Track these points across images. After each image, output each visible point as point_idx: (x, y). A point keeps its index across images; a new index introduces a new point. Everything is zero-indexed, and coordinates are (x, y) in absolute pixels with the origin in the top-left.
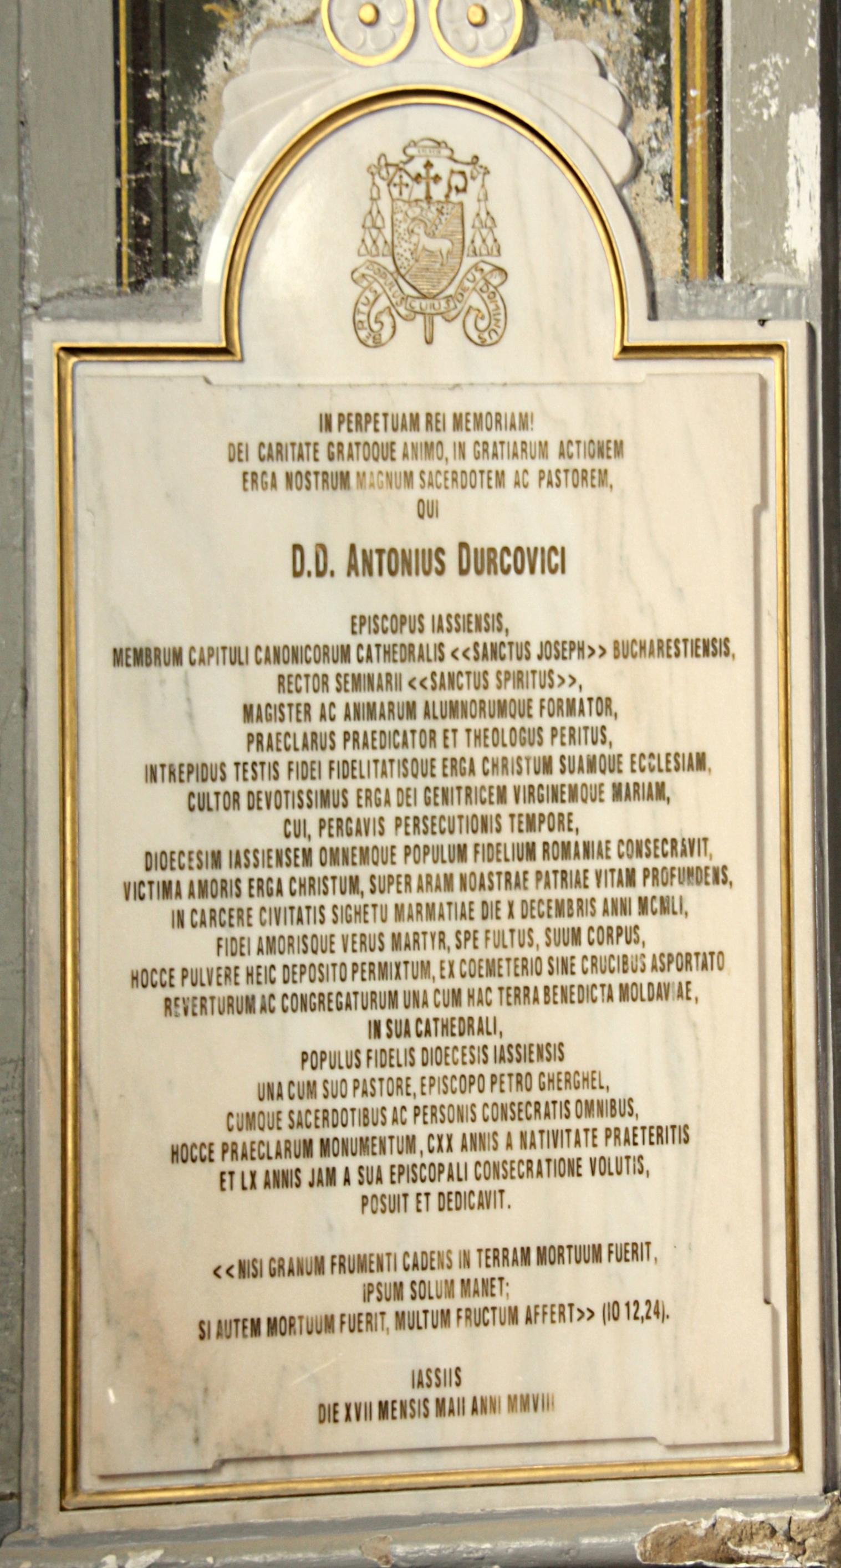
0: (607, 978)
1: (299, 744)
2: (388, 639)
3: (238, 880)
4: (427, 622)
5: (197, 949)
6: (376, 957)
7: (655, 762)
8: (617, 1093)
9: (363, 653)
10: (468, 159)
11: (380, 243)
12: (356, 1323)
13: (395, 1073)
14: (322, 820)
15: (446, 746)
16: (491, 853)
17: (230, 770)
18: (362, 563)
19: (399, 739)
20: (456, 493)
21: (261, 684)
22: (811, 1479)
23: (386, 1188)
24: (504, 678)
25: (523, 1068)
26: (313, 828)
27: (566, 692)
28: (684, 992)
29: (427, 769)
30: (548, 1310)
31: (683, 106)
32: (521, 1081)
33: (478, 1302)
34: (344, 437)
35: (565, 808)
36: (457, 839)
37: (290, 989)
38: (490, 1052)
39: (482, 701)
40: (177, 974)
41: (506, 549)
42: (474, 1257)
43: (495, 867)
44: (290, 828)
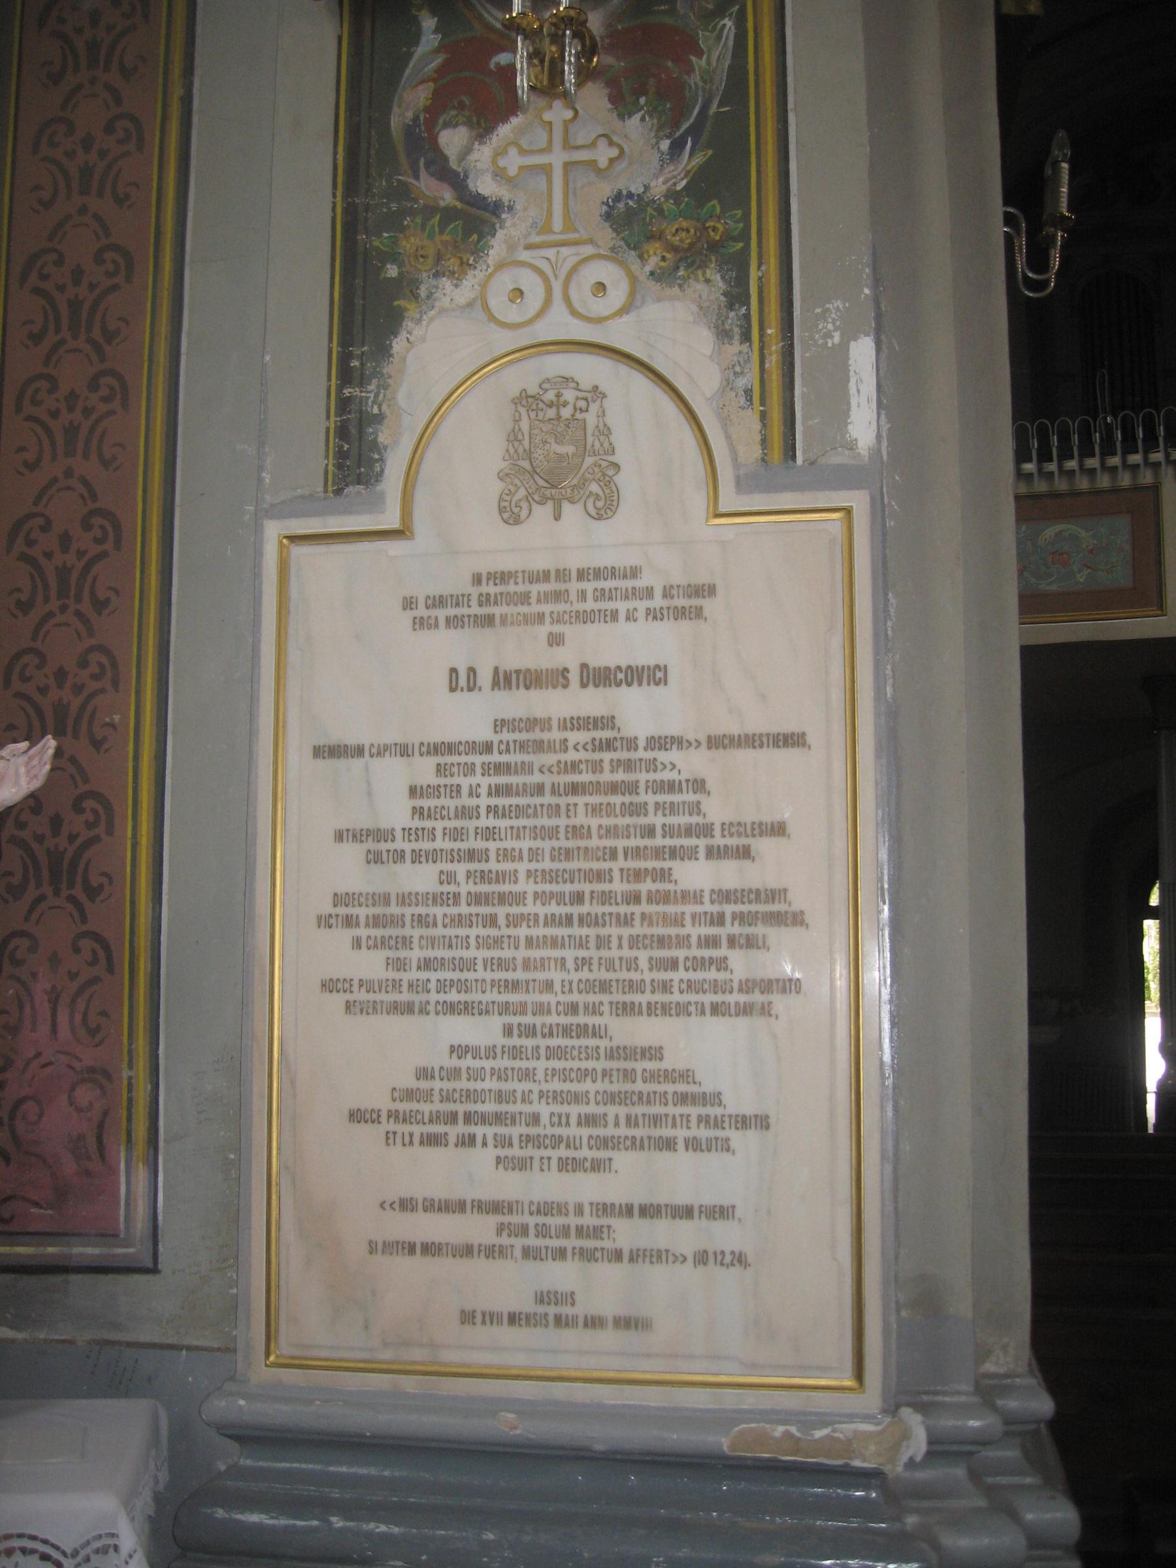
0: (701, 998)
1: (452, 814)
2: (524, 736)
3: (403, 915)
4: (555, 724)
5: (372, 965)
6: (510, 976)
7: (742, 829)
8: (708, 1087)
9: (503, 747)
10: (589, 388)
11: (521, 450)
12: (492, 1252)
13: (524, 1064)
14: (468, 872)
15: (568, 817)
16: (606, 898)
17: (399, 834)
18: (503, 680)
19: (530, 811)
20: (579, 628)
21: (425, 770)
22: (872, 1399)
23: (516, 1152)
24: (616, 765)
25: (629, 1065)
26: (461, 877)
27: (667, 775)
28: (765, 1010)
29: (552, 833)
30: (648, 1253)
31: (761, 341)
32: (628, 1075)
33: (590, 1244)
34: (492, 589)
35: (666, 865)
36: (576, 887)
37: (442, 997)
38: (602, 1051)
39: (598, 782)
40: (356, 983)
41: (619, 668)
42: (587, 1209)
43: (607, 909)
44: (444, 877)
